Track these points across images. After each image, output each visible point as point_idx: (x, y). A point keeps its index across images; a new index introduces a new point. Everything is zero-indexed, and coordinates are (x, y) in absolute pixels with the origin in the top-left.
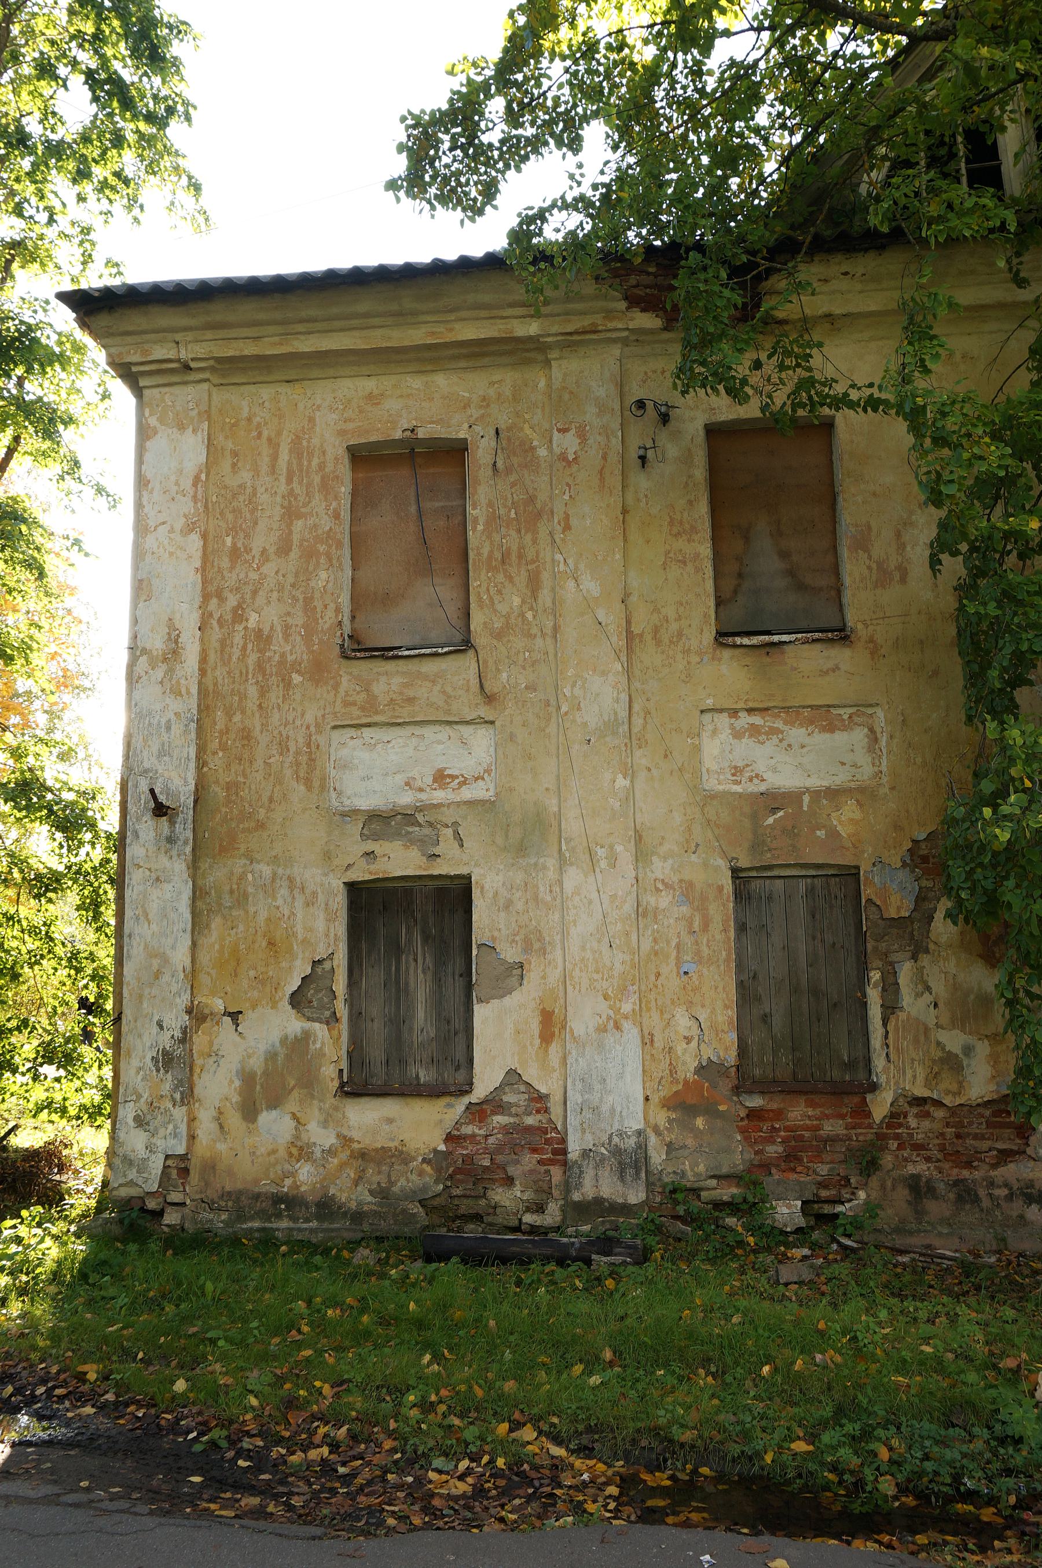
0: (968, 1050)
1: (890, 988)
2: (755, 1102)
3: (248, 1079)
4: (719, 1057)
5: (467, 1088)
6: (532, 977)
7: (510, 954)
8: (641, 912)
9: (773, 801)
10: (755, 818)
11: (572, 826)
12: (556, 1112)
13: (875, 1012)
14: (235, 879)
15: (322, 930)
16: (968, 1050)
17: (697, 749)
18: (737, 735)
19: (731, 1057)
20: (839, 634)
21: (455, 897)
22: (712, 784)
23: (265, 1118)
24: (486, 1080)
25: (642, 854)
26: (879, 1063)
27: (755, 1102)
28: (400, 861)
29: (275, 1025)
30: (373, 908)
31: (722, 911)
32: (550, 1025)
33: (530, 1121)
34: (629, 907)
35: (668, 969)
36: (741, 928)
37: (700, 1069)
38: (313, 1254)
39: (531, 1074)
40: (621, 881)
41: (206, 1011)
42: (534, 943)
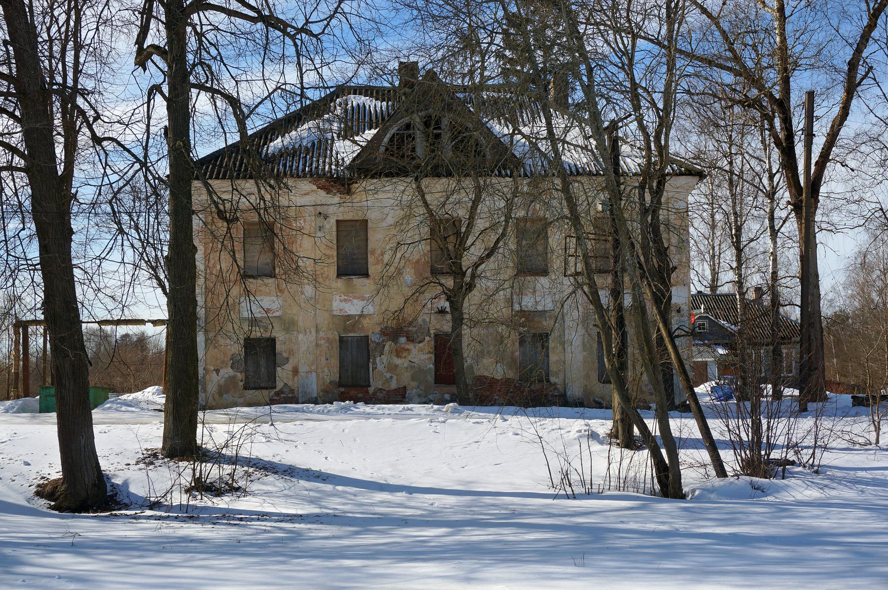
0: (391, 377)
1: (374, 363)
2: (342, 390)
3: (220, 386)
4: (97, 354)
5: (275, 387)
6: (291, 361)
7: (285, 355)
8: (317, 345)
9: (349, 317)
10: (345, 322)
11: (301, 324)
12: (296, 393)
13: (371, 369)
14: (622, 481)
15: (236, 348)
16: (391, 377)
17: (331, 305)
18: (341, 301)
19: (338, 380)
20: (366, 275)
21: (272, 341)
22: (335, 313)
23: (225, 396)
24: (279, 385)
25: (317, 331)
26: (371, 380)
27: (342, 390)
28: (257, 333)
29: (227, 372)
30: (250, 344)
31: (336, 345)
32: (295, 371)
33: (290, 395)
34: (314, 344)
35: (323, 359)
36: (341, 348)
37: (331, 382)
38: (769, 130)
39: (290, 384)
40: (312, 337)
41: (811, 406)
42: (291, 352)
